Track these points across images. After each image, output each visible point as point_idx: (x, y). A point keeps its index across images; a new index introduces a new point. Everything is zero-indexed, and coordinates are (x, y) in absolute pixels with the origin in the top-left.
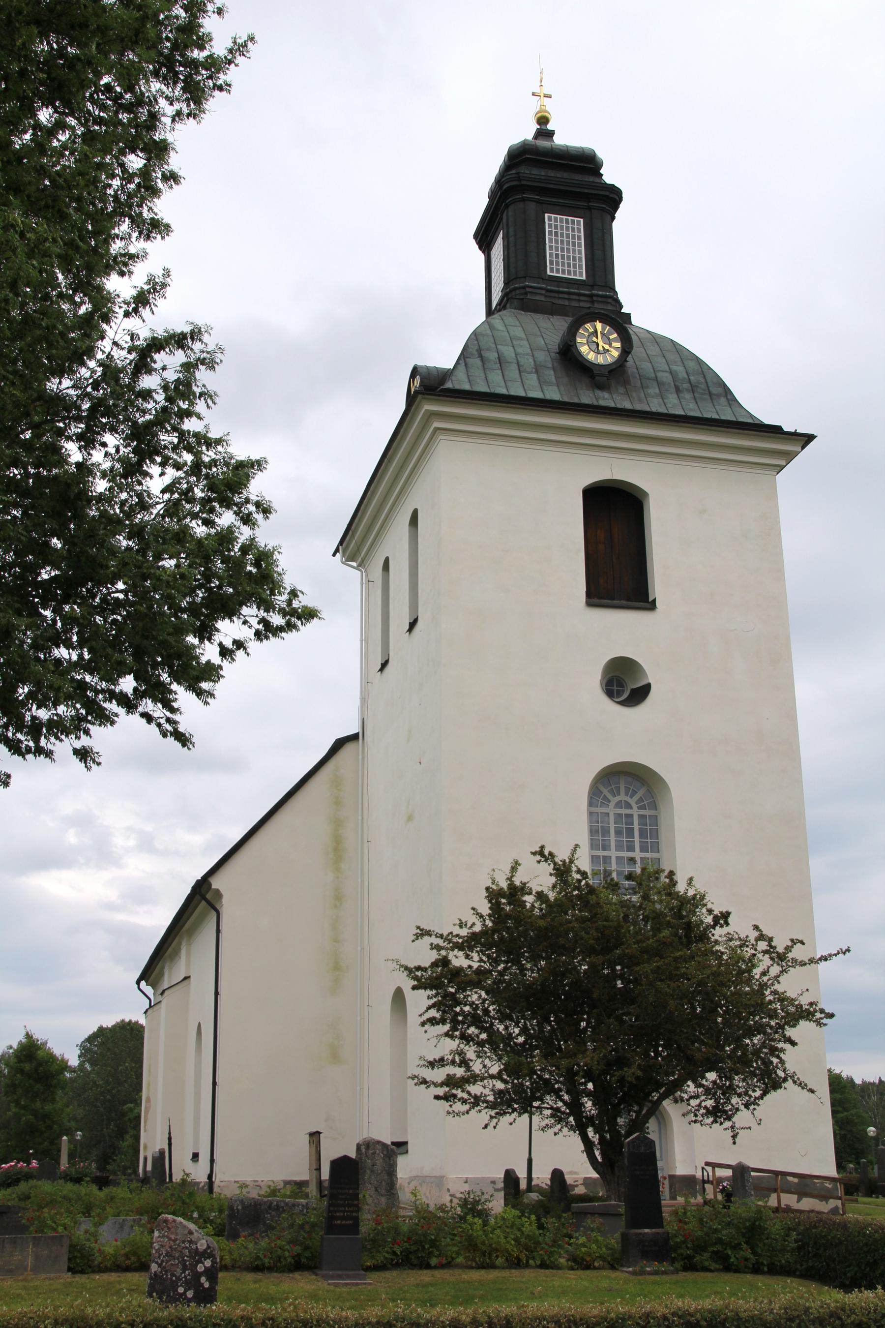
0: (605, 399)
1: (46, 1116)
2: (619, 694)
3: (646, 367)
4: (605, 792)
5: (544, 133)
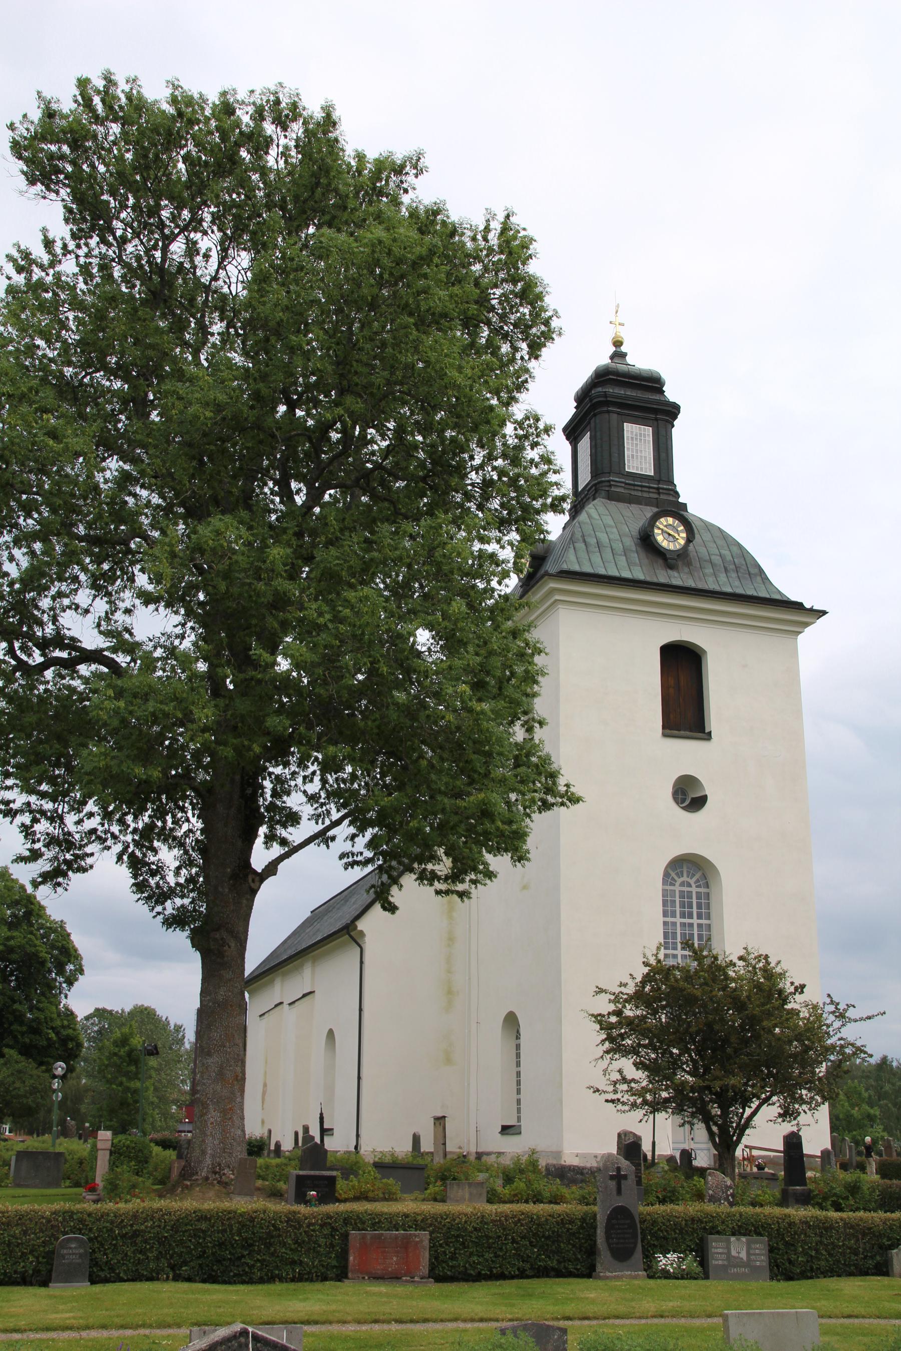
0: (676, 579)
1: (135, 1091)
2: (683, 801)
3: (702, 551)
4: (673, 874)
5: (618, 355)
